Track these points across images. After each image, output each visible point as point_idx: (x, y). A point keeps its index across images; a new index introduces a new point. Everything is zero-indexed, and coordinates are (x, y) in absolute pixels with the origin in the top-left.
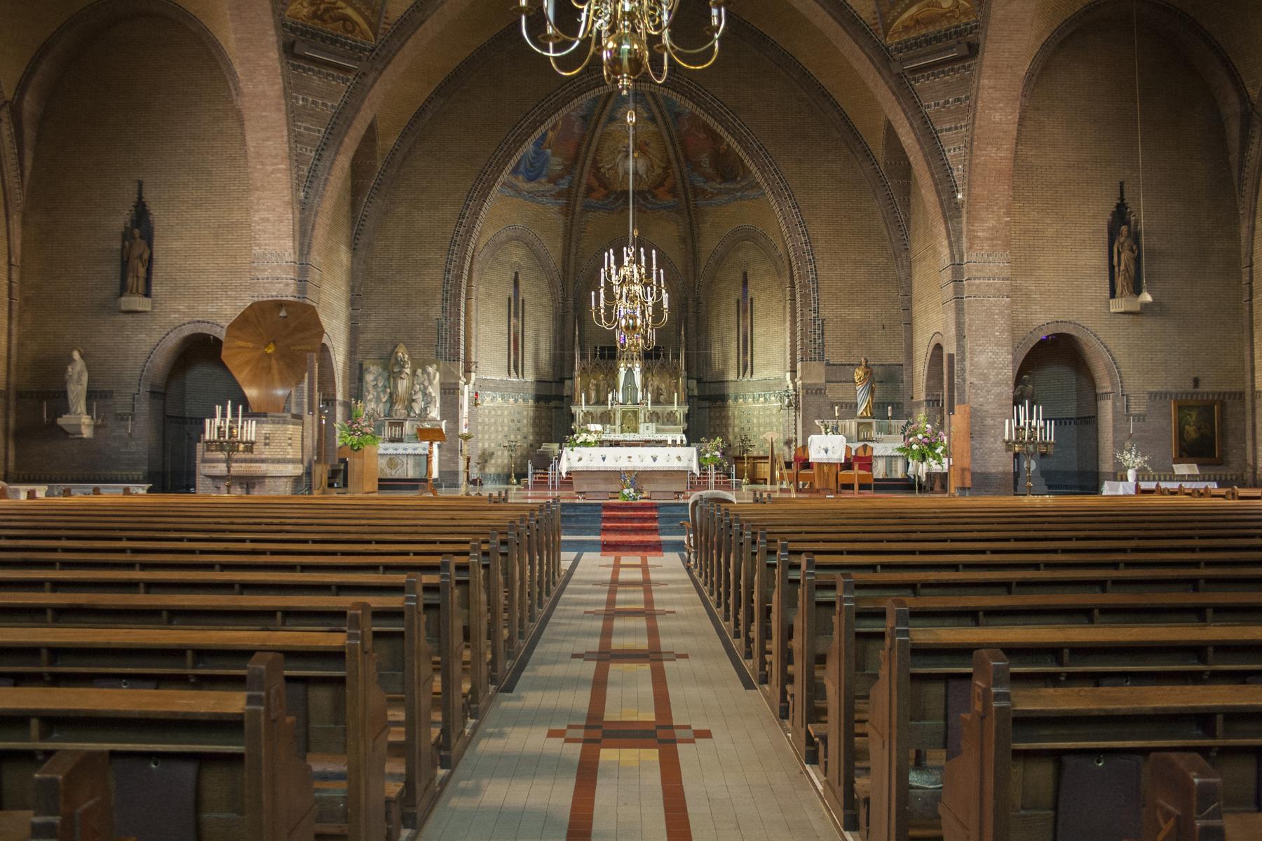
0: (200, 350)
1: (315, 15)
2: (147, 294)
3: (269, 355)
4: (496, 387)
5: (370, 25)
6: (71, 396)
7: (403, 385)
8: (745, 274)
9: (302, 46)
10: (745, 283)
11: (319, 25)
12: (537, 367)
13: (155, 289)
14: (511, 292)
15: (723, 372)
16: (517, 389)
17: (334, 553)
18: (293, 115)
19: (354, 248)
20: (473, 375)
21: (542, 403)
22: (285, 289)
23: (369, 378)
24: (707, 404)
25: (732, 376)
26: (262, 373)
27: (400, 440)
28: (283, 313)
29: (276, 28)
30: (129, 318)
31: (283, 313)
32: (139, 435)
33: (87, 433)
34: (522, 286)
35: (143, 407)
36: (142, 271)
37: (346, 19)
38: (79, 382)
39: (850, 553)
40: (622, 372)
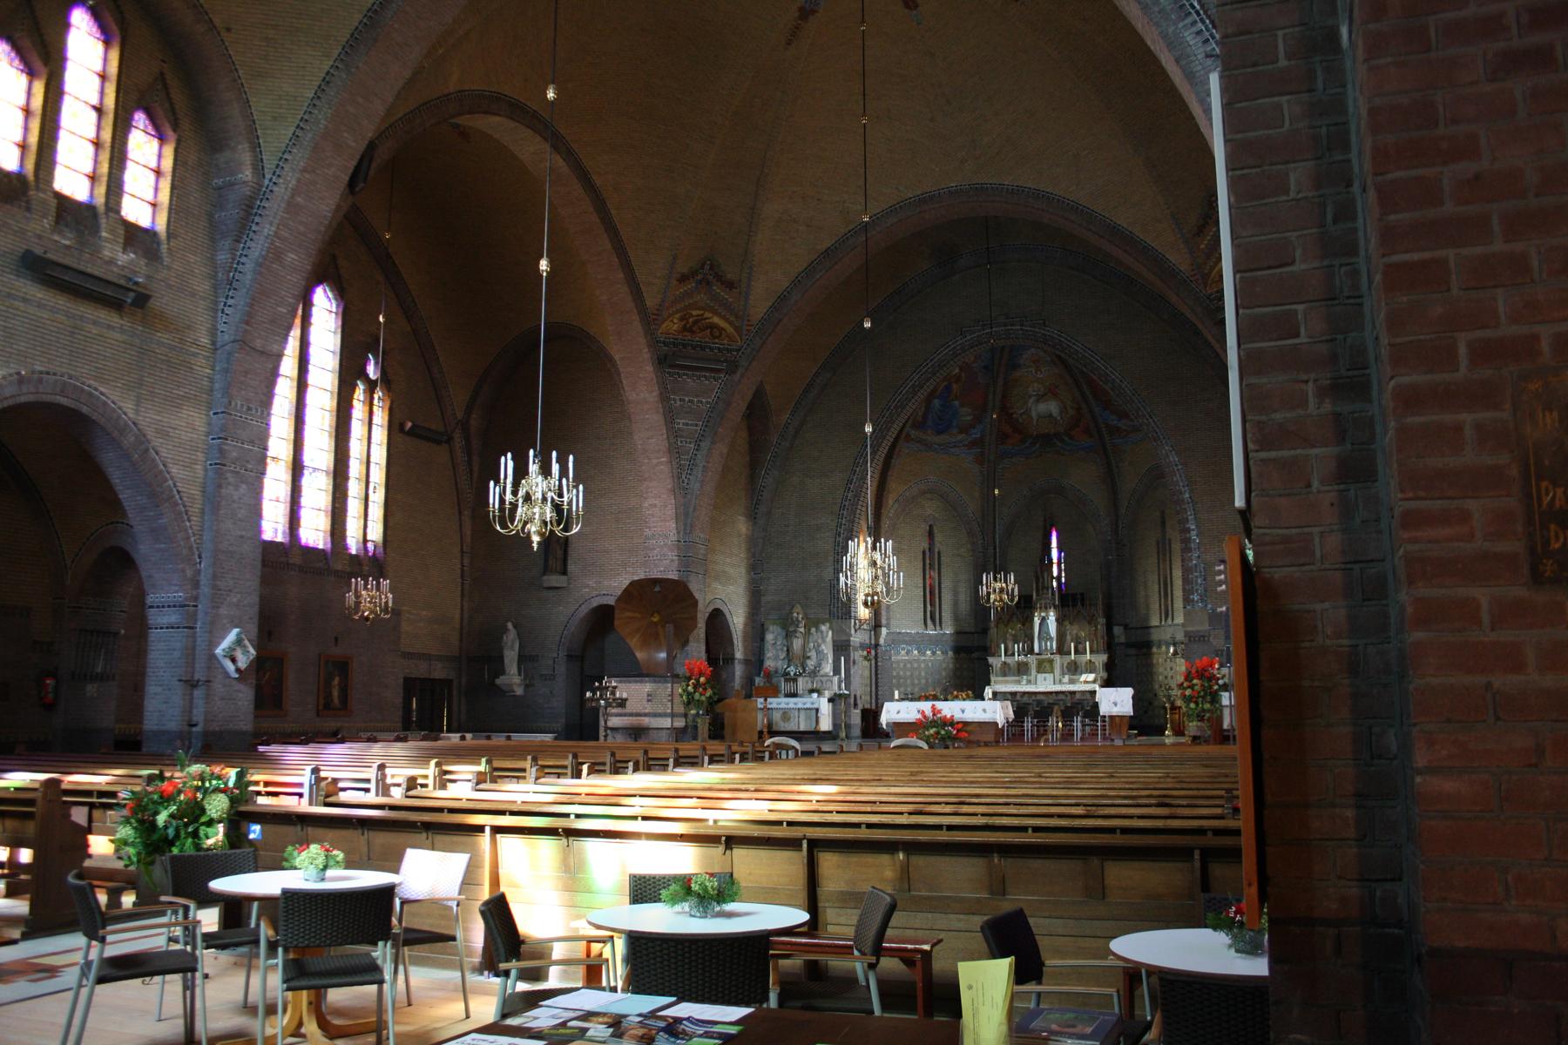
0: (602, 618)
1: (684, 329)
2: (564, 573)
3: (656, 624)
4: (911, 640)
5: (736, 328)
6: (506, 661)
7: (797, 644)
8: (1163, 513)
9: (670, 359)
10: (1163, 523)
11: (688, 336)
12: (956, 618)
13: (571, 567)
14: (926, 546)
15: (1147, 618)
16: (934, 642)
17: (1131, 817)
18: (670, 416)
19: (752, 516)
20: (884, 631)
21: (963, 655)
22: (665, 566)
23: (769, 637)
24: (1133, 651)
25: (1155, 621)
26: (651, 638)
27: (794, 695)
28: (657, 589)
29: (649, 346)
30: (551, 593)
31: (657, 589)
32: (556, 696)
33: (519, 691)
34: (938, 538)
35: (561, 669)
36: (560, 553)
37: (713, 327)
38: (512, 648)
39: (1060, 816)
40: (1037, 621)
